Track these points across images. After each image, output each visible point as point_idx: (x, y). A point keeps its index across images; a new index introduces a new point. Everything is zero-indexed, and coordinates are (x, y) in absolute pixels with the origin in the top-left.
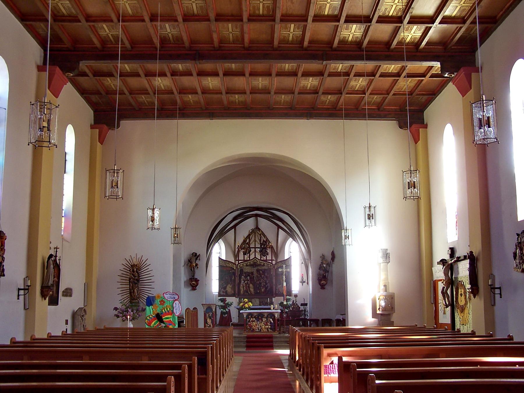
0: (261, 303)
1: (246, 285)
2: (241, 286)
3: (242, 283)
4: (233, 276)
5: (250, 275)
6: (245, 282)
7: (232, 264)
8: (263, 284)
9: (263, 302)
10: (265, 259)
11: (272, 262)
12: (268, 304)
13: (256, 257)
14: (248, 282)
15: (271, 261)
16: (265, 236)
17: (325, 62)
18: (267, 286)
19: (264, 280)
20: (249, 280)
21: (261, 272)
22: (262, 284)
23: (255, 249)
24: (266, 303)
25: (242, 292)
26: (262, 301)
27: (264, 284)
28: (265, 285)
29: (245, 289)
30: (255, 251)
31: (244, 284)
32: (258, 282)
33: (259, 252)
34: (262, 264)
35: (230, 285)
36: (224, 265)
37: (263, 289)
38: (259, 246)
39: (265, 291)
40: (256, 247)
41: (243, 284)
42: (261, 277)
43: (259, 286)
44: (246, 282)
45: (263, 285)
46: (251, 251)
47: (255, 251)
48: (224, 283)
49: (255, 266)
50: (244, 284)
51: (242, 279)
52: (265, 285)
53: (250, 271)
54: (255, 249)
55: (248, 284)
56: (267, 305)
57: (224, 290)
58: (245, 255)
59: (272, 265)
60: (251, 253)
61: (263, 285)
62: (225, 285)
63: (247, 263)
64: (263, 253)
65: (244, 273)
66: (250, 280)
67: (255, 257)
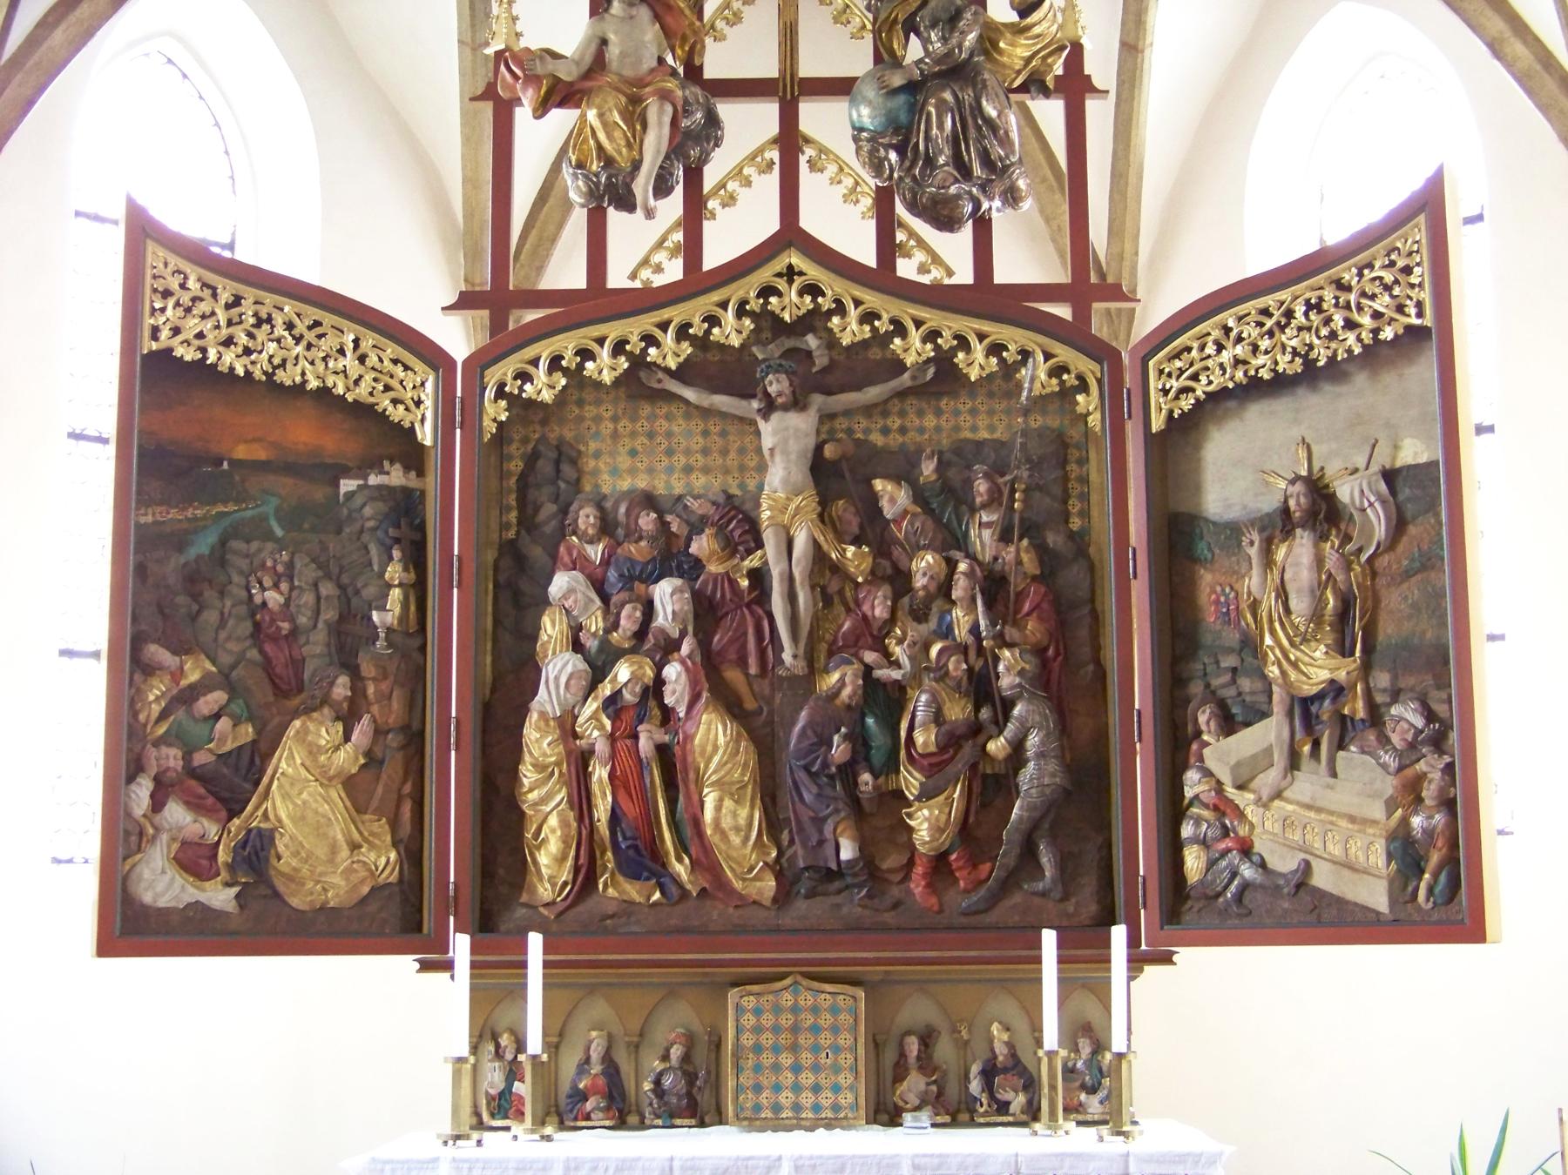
0: (899, 1075)
1: (622, 736)
2: (539, 742)
3: (547, 699)
4: (394, 572)
5: (702, 545)
6: (598, 671)
7: (369, 340)
8: (938, 718)
9: (944, 1051)
10: (964, 275)
11: (1082, 314)
12: (1030, 1085)
13: (809, 222)
14: (659, 682)
15: (1063, 311)
16: (760, 151)
17: (637, 284)
18: (997, 746)
19: (946, 632)
20: (685, 649)
21: (893, 497)
22: (921, 702)
23: (789, 118)
24: (990, 1073)
25: (561, 859)
26: (927, 1039)
27: (957, 711)
28: (976, 731)
29: (602, 811)
30: (790, 140)
31: (592, 706)
32: (840, 680)
33: (846, 151)
34: (913, 350)
35: (325, 732)
36: (229, 357)
37: (926, 795)
38: (856, 59)
39: (965, 830)
40: (806, 69)
41: (567, 727)
42: (900, 581)
43: (860, 740)
44: (623, 672)
45: (924, 739)
46: (712, 126)
47: (790, 140)
48: (217, 697)
49: (776, 385)
50: (592, 706)
51: (552, 628)
52: (976, 731)
53: (699, 482)
54: (789, 118)
55: (667, 714)
56: (1018, 1101)
57: (212, 830)
58: (614, 217)
59: (1082, 364)
60: (711, 176)
61: (924, 739)
62: (231, 735)
63: (713, 321)
64: (930, 162)
65: (586, 518)
66: (704, 643)
67: (790, 234)
